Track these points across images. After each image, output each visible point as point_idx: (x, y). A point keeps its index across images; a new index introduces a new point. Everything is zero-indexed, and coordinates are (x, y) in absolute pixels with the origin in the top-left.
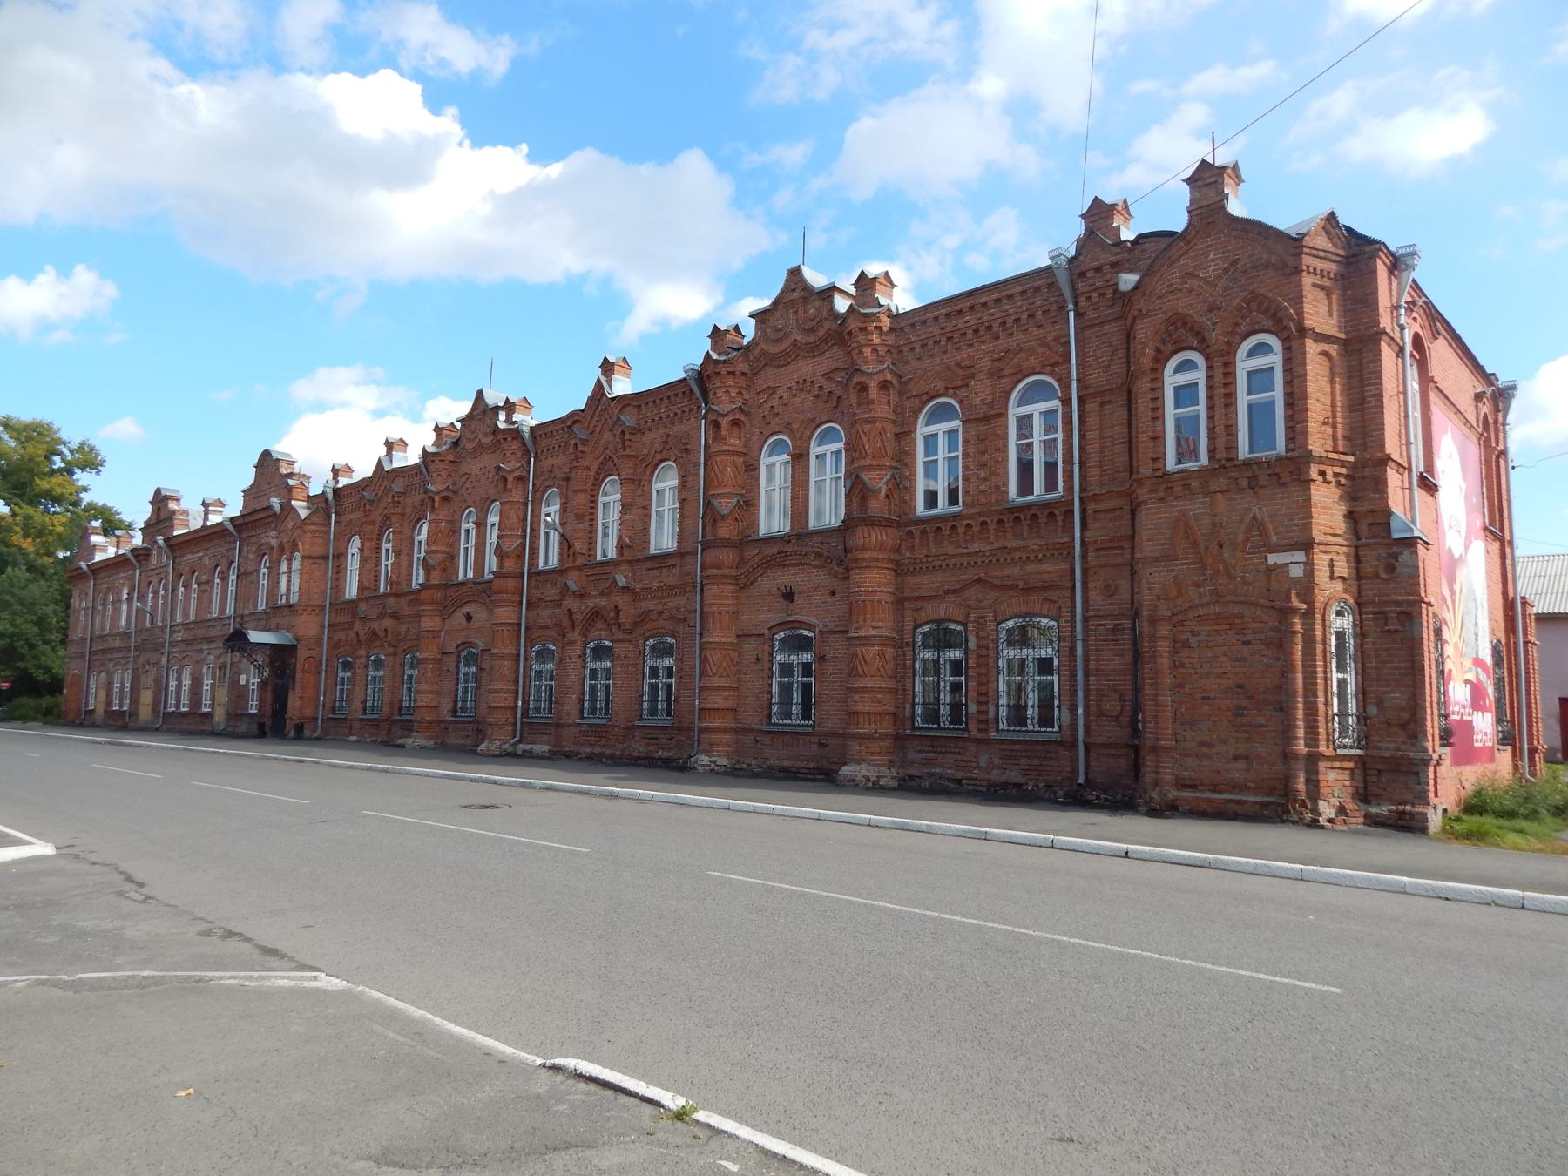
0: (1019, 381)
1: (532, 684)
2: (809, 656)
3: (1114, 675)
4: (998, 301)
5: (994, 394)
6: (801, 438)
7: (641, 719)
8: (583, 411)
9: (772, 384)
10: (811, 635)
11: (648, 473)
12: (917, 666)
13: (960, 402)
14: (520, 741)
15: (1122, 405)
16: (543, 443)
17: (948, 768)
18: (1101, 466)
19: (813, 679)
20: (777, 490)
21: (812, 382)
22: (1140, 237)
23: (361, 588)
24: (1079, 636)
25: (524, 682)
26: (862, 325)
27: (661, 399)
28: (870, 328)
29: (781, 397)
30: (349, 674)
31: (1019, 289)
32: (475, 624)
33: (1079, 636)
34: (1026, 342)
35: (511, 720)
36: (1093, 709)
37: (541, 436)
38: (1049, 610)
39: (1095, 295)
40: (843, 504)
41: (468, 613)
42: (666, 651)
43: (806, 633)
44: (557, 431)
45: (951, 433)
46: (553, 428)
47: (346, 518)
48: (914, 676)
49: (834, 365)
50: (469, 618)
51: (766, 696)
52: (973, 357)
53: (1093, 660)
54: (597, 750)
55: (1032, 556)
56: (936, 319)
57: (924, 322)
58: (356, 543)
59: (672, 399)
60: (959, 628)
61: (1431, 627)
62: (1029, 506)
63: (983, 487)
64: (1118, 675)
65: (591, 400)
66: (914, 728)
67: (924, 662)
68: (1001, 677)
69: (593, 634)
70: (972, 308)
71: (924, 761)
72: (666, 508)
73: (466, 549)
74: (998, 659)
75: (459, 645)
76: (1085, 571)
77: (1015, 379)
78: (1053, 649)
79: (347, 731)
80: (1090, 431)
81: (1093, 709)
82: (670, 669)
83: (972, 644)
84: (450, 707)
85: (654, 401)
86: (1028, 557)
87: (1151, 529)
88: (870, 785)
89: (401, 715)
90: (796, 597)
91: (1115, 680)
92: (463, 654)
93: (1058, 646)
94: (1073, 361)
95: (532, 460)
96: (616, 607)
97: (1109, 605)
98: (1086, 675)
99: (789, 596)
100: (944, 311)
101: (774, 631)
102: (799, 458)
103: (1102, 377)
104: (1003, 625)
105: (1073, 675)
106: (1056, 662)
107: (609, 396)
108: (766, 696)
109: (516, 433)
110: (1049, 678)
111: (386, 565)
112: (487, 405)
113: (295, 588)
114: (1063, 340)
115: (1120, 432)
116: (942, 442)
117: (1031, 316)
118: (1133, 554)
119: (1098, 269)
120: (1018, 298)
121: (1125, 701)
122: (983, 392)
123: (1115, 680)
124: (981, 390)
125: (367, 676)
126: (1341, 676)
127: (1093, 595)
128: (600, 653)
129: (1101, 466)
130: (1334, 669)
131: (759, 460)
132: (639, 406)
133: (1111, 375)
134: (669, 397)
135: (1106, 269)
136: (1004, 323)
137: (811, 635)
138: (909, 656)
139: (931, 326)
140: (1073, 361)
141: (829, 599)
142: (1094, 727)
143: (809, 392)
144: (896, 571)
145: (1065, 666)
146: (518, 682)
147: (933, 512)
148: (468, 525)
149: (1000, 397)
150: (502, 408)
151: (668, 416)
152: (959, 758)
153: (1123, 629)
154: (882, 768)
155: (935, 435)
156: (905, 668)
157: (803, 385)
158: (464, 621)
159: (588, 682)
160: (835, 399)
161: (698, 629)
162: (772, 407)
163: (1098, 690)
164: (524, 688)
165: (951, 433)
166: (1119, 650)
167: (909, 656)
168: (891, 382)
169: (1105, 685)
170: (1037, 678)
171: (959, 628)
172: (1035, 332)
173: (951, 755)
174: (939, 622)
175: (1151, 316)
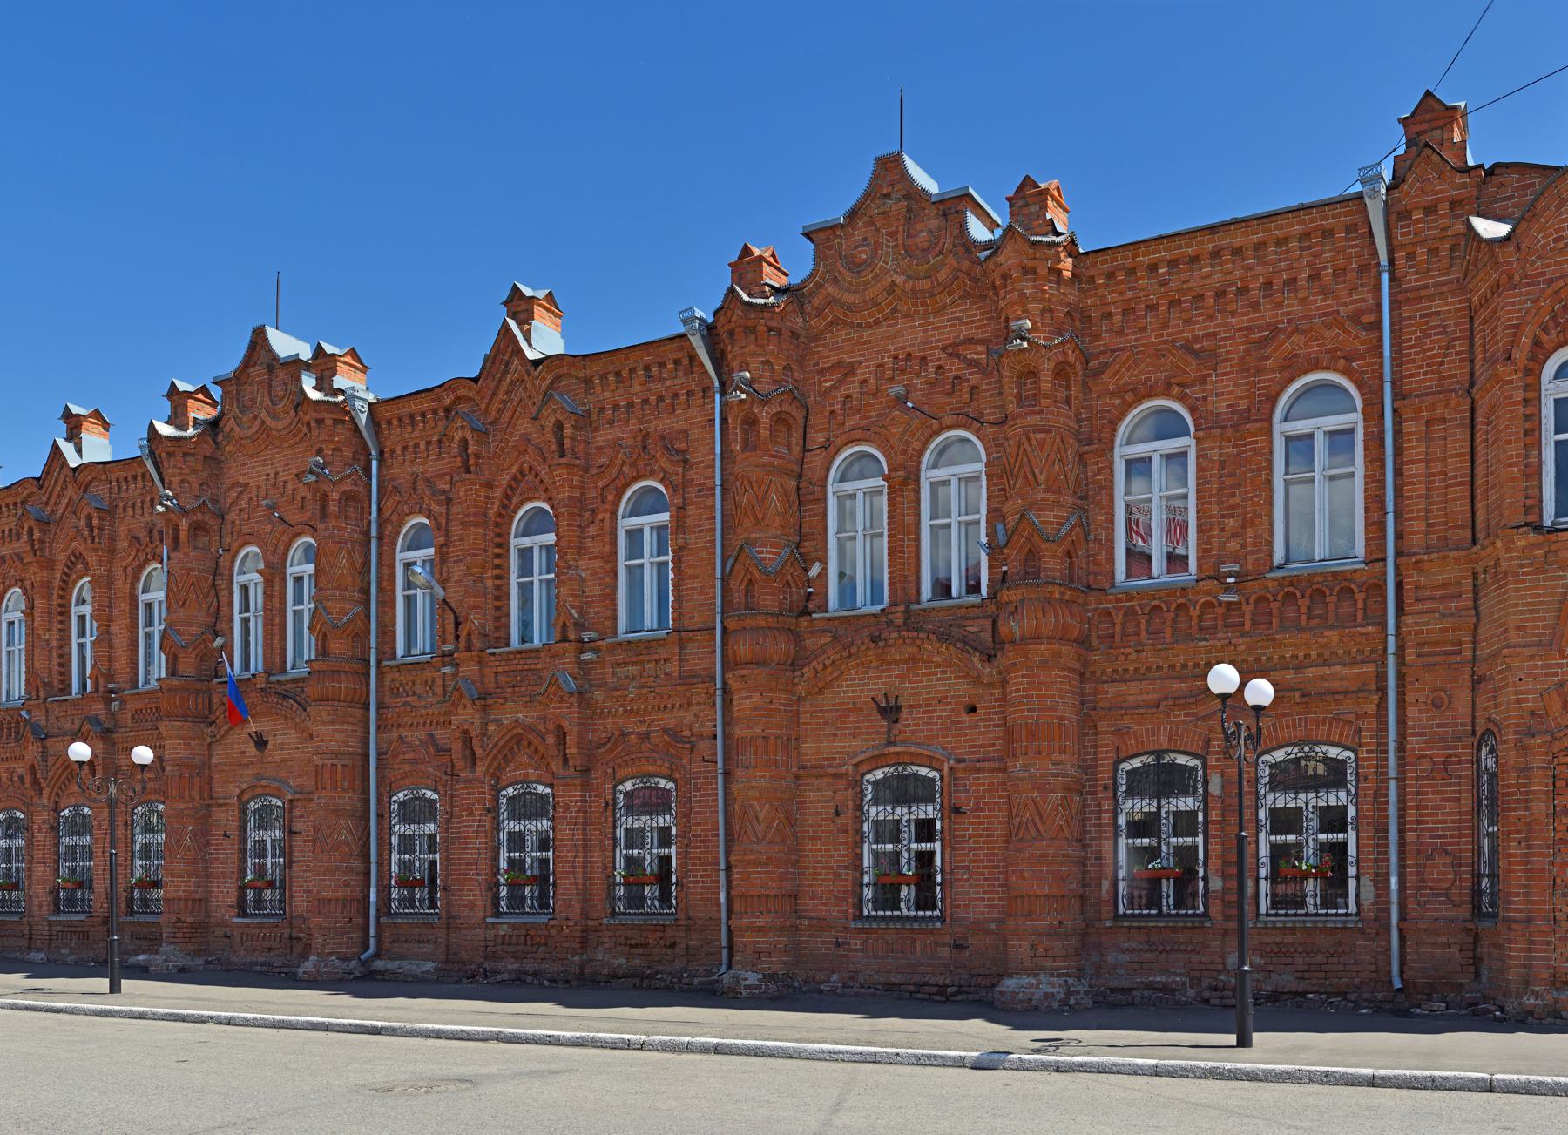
0: (1291, 380)
1: (394, 857)
2: (930, 808)
3: (1443, 829)
4: (1260, 246)
5: (1250, 396)
6: (904, 452)
7: (614, 914)
8: (475, 380)
9: (847, 359)
10: (933, 774)
11: (610, 497)
12: (866, 827)
13: (1193, 410)
14: (377, 955)
15: (1462, 426)
16: (393, 440)
17: (1176, 974)
18: (1427, 518)
19: (938, 845)
20: (860, 536)
21: (924, 358)
22: (1497, 165)
23: (267, 659)
24: (1392, 773)
25: (380, 855)
26: (1030, 264)
27: (632, 371)
28: (1043, 271)
29: (864, 382)
30: (19, 842)
31: (1298, 229)
32: (274, 753)
33: (1392, 773)
34: (1305, 317)
35: (359, 920)
36: (1412, 879)
37: (389, 423)
38: (1341, 735)
39: (1421, 252)
40: (23, 669)
41: (259, 734)
42: (661, 803)
43: (923, 771)
44: (423, 415)
45: (659, 529)
46: (411, 407)
47: (402, 471)
48: (1116, 836)
49: (964, 332)
50: (261, 743)
51: (851, 875)
52: (1214, 335)
53: (1412, 808)
54: (530, 966)
55: (1314, 654)
56: (1153, 268)
57: (1131, 272)
58: (83, 585)
59: (655, 370)
60: (1193, 762)
61: (157, 629)
62: (1142, 593)
63: (1233, 545)
64: (1448, 829)
65: (490, 360)
66: (1116, 917)
67: (876, 823)
68: (866, 846)
69: (510, 772)
70: (1216, 254)
71: (1136, 966)
72: (536, 578)
73: (246, 621)
74: (1257, 808)
75: (243, 792)
76: (1401, 677)
77: (1287, 375)
78: (1348, 792)
79: (25, 943)
80: (1411, 462)
81: (1412, 879)
82: (432, 837)
83: (1215, 787)
84: (233, 897)
85: (618, 374)
86: (1307, 656)
87: (1522, 613)
88: (1056, 1005)
89: (132, 913)
90: (904, 714)
91: (1445, 836)
92: (253, 805)
93: (1357, 789)
94: (1387, 353)
95: (374, 464)
96: (559, 727)
97: (1439, 726)
98: (1402, 831)
99: (891, 711)
100: (1169, 255)
101: (862, 770)
102: (903, 484)
103: (1431, 380)
104: (1267, 758)
105: (1382, 831)
106: (1352, 812)
107: (531, 355)
108: (851, 875)
109: (340, 411)
110: (1341, 836)
111: (81, 646)
112: (275, 357)
113: (300, 608)
114: (1368, 319)
115: (1457, 466)
116: (537, 560)
117: (1315, 276)
118: (1474, 651)
119: (1430, 210)
120: (1227, 256)
121: (1460, 866)
122: (1231, 393)
123: (1445, 836)
124: (1229, 393)
125: (57, 845)
126: (246, 615)
127: (1411, 712)
128: (527, 807)
129: (1427, 518)
130: (1352, 851)
131: (824, 487)
132: (588, 381)
133: (1443, 378)
134: (647, 368)
135: (1444, 209)
136: (1268, 285)
137: (933, 774)
138: (1107, 806)
139: (1141, 278)
140: (1387, 353)
141: (965, 717)
142: (1411, 905)
143: (918, 375)
144: (1082, 675)
145: (1366, 817)
146: (368, 855)
147: (527, 646)
148: (248, 574)
149: (908, 546)
150: (307, 366)
151: (645, 401)
152: (1194, 958)
153: (1460, 762)
154: (1070, 981)
155: (640, 531)
156: (1100, 825)
157: (905, 362)
158: (251, 750)
159: (504, 855)
160: (967, 390)
161: (720, 765)
162: (848, 397)
163: (1419, 852)
164: (379, 864)
165: (1340, 440)
166: (1452, 792)
167: (1107, 806)
168: (1073, 366)
169: (1429, 844)
170: (914, 846)
171: (1193, 762)
172: (1319, 301)
173: (1179, 955)
174: (1159, 754)
175: (1529, 285)
